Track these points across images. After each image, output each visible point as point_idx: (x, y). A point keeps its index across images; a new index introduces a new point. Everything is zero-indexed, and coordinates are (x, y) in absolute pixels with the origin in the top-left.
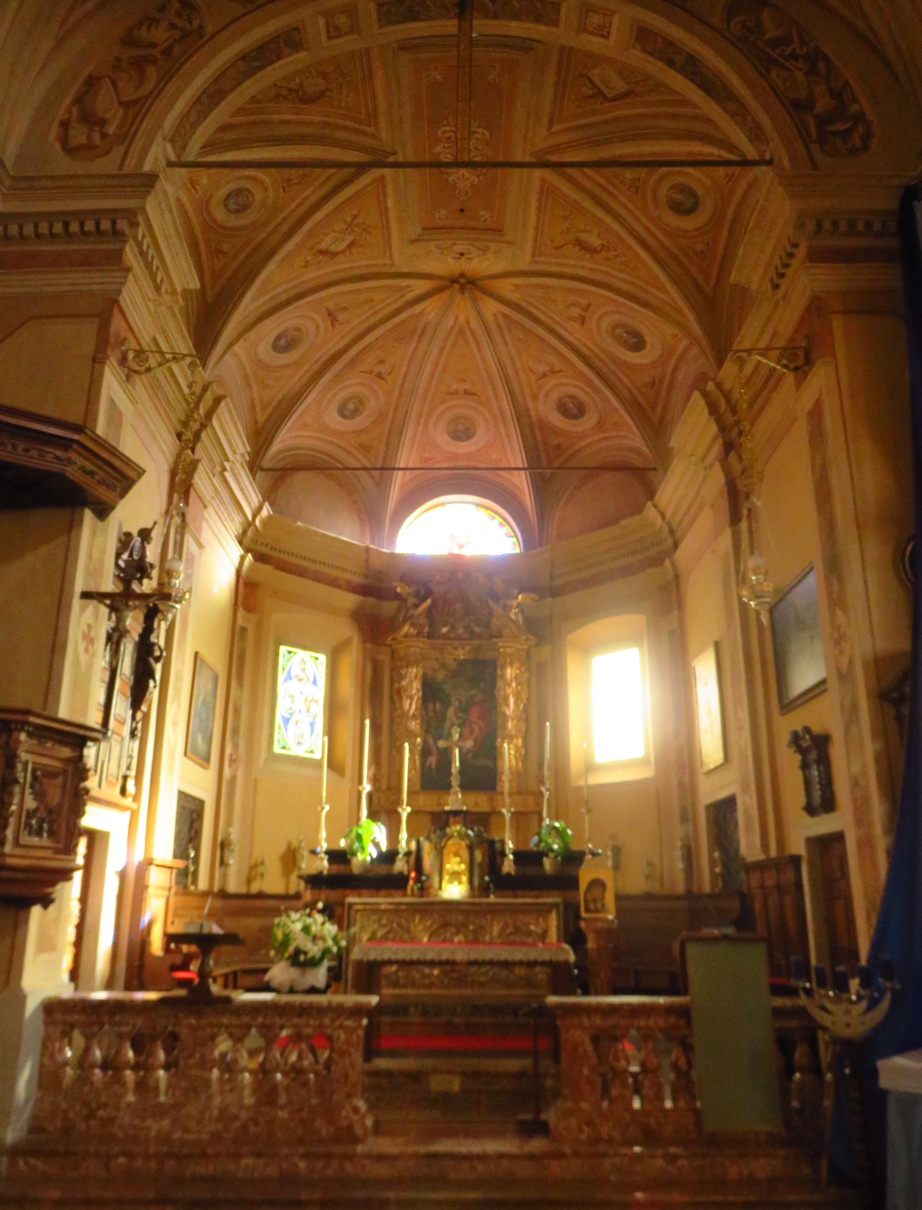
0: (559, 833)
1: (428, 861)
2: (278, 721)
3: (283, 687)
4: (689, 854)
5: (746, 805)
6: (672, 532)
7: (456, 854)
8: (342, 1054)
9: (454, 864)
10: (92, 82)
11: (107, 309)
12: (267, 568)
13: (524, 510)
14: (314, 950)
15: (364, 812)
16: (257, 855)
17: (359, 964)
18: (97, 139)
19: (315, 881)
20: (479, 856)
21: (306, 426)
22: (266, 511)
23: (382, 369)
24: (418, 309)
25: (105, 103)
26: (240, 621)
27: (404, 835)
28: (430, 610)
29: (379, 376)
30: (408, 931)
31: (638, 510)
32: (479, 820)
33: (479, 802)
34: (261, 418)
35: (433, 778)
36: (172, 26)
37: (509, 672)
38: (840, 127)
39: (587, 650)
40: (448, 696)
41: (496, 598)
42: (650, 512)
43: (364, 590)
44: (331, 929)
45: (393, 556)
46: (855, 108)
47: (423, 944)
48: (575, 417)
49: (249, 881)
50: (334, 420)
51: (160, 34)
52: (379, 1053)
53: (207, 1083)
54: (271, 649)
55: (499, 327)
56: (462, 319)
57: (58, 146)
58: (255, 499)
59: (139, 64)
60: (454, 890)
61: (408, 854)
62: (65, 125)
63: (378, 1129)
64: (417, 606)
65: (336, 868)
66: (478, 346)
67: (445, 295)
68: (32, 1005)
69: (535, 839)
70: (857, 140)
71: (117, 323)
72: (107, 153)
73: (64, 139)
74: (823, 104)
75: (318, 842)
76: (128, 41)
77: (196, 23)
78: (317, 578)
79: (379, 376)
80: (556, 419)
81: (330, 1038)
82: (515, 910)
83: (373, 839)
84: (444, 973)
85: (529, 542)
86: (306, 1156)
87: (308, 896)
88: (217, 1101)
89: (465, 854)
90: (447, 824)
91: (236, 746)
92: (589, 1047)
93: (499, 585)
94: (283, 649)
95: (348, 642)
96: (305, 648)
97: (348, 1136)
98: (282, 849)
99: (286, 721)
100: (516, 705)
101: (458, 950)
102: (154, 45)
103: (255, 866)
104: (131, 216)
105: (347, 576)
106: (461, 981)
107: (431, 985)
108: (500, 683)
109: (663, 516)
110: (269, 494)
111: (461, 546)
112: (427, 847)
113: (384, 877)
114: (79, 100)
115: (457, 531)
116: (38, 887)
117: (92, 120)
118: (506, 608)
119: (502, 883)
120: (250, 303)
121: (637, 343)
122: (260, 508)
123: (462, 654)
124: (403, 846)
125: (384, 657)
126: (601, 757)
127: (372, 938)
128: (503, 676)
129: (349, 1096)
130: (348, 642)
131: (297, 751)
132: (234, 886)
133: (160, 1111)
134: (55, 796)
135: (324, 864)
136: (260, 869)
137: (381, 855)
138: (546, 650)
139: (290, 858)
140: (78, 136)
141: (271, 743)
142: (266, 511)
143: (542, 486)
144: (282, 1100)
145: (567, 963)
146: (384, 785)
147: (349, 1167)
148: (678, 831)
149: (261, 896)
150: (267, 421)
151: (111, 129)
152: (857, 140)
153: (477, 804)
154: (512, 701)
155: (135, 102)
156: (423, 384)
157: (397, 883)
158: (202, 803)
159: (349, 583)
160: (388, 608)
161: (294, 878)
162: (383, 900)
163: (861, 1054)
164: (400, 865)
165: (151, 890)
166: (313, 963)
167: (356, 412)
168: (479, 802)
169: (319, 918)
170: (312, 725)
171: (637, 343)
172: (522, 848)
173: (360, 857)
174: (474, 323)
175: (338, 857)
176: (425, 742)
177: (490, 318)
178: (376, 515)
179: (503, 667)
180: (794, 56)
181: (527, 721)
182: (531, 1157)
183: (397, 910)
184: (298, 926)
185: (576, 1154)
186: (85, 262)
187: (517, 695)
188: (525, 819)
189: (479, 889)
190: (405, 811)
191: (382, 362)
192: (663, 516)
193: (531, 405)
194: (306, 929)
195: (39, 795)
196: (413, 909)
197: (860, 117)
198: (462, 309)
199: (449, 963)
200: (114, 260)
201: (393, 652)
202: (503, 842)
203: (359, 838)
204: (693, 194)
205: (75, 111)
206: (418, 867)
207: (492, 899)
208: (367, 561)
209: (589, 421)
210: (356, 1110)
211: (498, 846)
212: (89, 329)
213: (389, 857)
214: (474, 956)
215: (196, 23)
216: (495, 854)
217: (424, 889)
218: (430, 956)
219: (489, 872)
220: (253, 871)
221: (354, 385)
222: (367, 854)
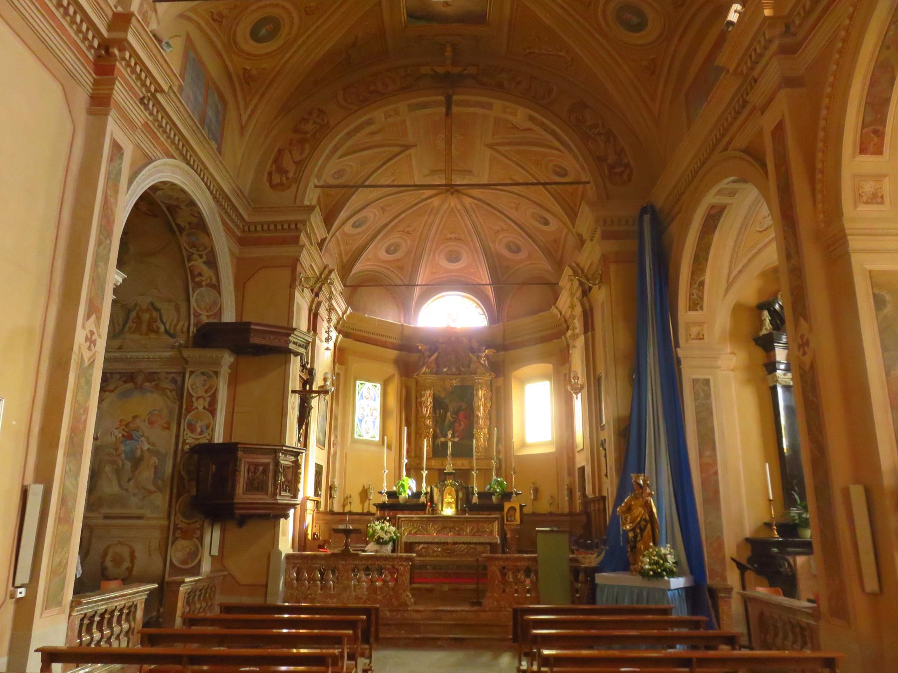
0: (500, 484)
1: (436, 497)
2: (356, 420)
3: (359, 403)
4: (571, 492)
5: (588, 470)
6: (566, 321)
7: (450, 494)
8: (402, 575)
9: (449, 499)
10: (280, 151)
11: (294, 264)
12: (349, 341)
13: (490, 301)
14: (386, 537)
15: (404, 473)
16: (348, 493)
17: (406, 543)
18: (285, 181)
19: (382, 507)
20: (461, 495)
21: (368, 260)
22: (349, 310)
23: (410, 229)
24: (429, 201)
25: (288, 163)
26: (336, 370)
27: (424, 485)
28: (437, 359)
29: (408, 232)
30: (427, 531)
31: (549, 307)
32: (462, 475)
33: (462, 463)
34: (345, 260)
35: (438, 451)
36: (315, 122)
37: (480, 393)
38: (618, 170)
39: (522, 382)
40: (447, 406)
41: (473, 351)
42: (554, 310)
43: (400, 348)
44: (393, 529)
45: (415, 328)
46: (625, 161)
47: (433, 535)
48: (516, 253)
49: (344, 506)
50: (382, 255)
51: (310, 127)
52: (414, 583)
53: (349, 586)
54: (352, 381)
55: (473, 209)
56: (452, 205)
57: (268, 184)
58: (344, 306)
59: (302, 142)
60: (449, 511)
61: (426, 494)
62: (270, 174)
63: (415, 603)
64: (430, 356)
65: (393, 501)
66: (461, 216)
67: (443, 196)
68: (283, 556)
69: (488, 487)
70: (625, 176)
71: (299, 267)
72: (289, 187)
73: (270, 180)
74: (611, 159)
75: (382, 488)
76: (296, 131)
77: (325, 121)
78: (376, 343)
79: (408, 232)
80: (506, 253)
81: (397, 569)
82: (478, 521)
83: (409, 485)
84: (444, 550)
85: (492, 320)
86: (390, 611)
87: (378, 514)
88: (353, 593)
89: (454, 494)
90: (445, 480)
91: (336, 436)
92: (498, 573)
93: (475, 345)
94: (358, 382)
95: (392, 377)
96: (369, 381)
97: (405, 604)
98: (360, 489)
99: (361, 421)
100: (484, 410)
101: (449, 537)
102: (307, 133)
103: (347, 498)
104: (304, 223)
105: (392, 340)
106: (451, 553)
107: (438, 556)
108: (475, 399)
109: (561, 313)
110: (349, 302)
111: (454, 321)
112: (435, 490)
113: (415, 505)
114: (276, 161)
115: (452, 313)
116: (282, 512)
117: (282, 171)
118: (479, 357)
119: (473, 508)
120: (343, 215)
121: (546, 223)
122: (346, 310)
123: (454, 383)
124: (424, 490)
125: (412, 385)
126: (529, 440)
127: (410, 533)
128: (477, 395)
129: (405, 591)
130: (392, 377)
131: (367, 437)
132: (336, 509)
133: (331, 597)
134: (290, 476)
135: (385, 499)
136: (349, 500)
137: (413, 493)
138: (500, 381)
139: (364, 494)
140: (276, 179)
141: (353, 433)
142: (349, 310)
143: (499, 293)
144: (379, 592)
145: (496, 543)
146: (413, 454)
147: (406, 615)
148: (567, 480)
149: (351, 513)
150: (348, 261)
151: (291, 175)
152: (625, 176)
153: (463, 465)
154: (482, 408)
155: (300, 161)
156: (431, 236)
157: (422, 507)
158: (322, 466)
159: (392, 344)
160: (414, 357)
161: (366, 504)
162: (415, 516)
163: (591, 572)
164: (423, 499)
165: (308, 512)
166: (386, 543)
167: (395, 251)
168: (462, 463)
169: (388, 524)
170: (374, 422)
171: (546, 223)
172: (482, 490)
173: (403, 495)
174: (459, 207)
175: (392, 495)
176: (434, 431)
177: (468, 205)
178: (404, 305)
179: (477, 390)
180: (599, 134)
181: (490, 419)
182: (474, 611)
183: (421, 520)
184: (379, 527)
185: (490, 610)
186: (284, 242)
187: (485, 406)
188: (485, 473)
189: (460, 510)
190: (425, 473)
191: (410, 226)
192: (561, 313)
193: (491, 245)
194: (382, 529)
195: (285, 476)
196: (429, 520)
197: (627, 166)
198: (453, 201)
199: (446, 543)
200: (296, 240)
201: (417, 382)
202: (473, 488)
203: (403, 486)
204: (564, 169)
205: (274, 167)
206: (431, 500)
207: (467, 515)
208: (402, 332)
209: (523, 255)
210: (407, 596)
211: (470, 489)
212: (287, 272)
213: (417, 495)
214: (456, 540)
215: (325, 121)
216: (468, 493)
217: (434, 510)
218: (437, 540)
219: (465, 504)
220: (346, 501)
221: (394, 238)
222: (406, 494)
